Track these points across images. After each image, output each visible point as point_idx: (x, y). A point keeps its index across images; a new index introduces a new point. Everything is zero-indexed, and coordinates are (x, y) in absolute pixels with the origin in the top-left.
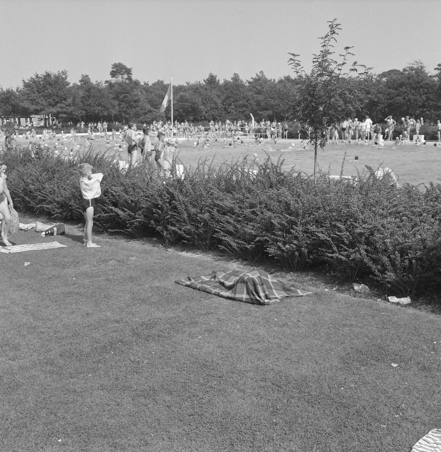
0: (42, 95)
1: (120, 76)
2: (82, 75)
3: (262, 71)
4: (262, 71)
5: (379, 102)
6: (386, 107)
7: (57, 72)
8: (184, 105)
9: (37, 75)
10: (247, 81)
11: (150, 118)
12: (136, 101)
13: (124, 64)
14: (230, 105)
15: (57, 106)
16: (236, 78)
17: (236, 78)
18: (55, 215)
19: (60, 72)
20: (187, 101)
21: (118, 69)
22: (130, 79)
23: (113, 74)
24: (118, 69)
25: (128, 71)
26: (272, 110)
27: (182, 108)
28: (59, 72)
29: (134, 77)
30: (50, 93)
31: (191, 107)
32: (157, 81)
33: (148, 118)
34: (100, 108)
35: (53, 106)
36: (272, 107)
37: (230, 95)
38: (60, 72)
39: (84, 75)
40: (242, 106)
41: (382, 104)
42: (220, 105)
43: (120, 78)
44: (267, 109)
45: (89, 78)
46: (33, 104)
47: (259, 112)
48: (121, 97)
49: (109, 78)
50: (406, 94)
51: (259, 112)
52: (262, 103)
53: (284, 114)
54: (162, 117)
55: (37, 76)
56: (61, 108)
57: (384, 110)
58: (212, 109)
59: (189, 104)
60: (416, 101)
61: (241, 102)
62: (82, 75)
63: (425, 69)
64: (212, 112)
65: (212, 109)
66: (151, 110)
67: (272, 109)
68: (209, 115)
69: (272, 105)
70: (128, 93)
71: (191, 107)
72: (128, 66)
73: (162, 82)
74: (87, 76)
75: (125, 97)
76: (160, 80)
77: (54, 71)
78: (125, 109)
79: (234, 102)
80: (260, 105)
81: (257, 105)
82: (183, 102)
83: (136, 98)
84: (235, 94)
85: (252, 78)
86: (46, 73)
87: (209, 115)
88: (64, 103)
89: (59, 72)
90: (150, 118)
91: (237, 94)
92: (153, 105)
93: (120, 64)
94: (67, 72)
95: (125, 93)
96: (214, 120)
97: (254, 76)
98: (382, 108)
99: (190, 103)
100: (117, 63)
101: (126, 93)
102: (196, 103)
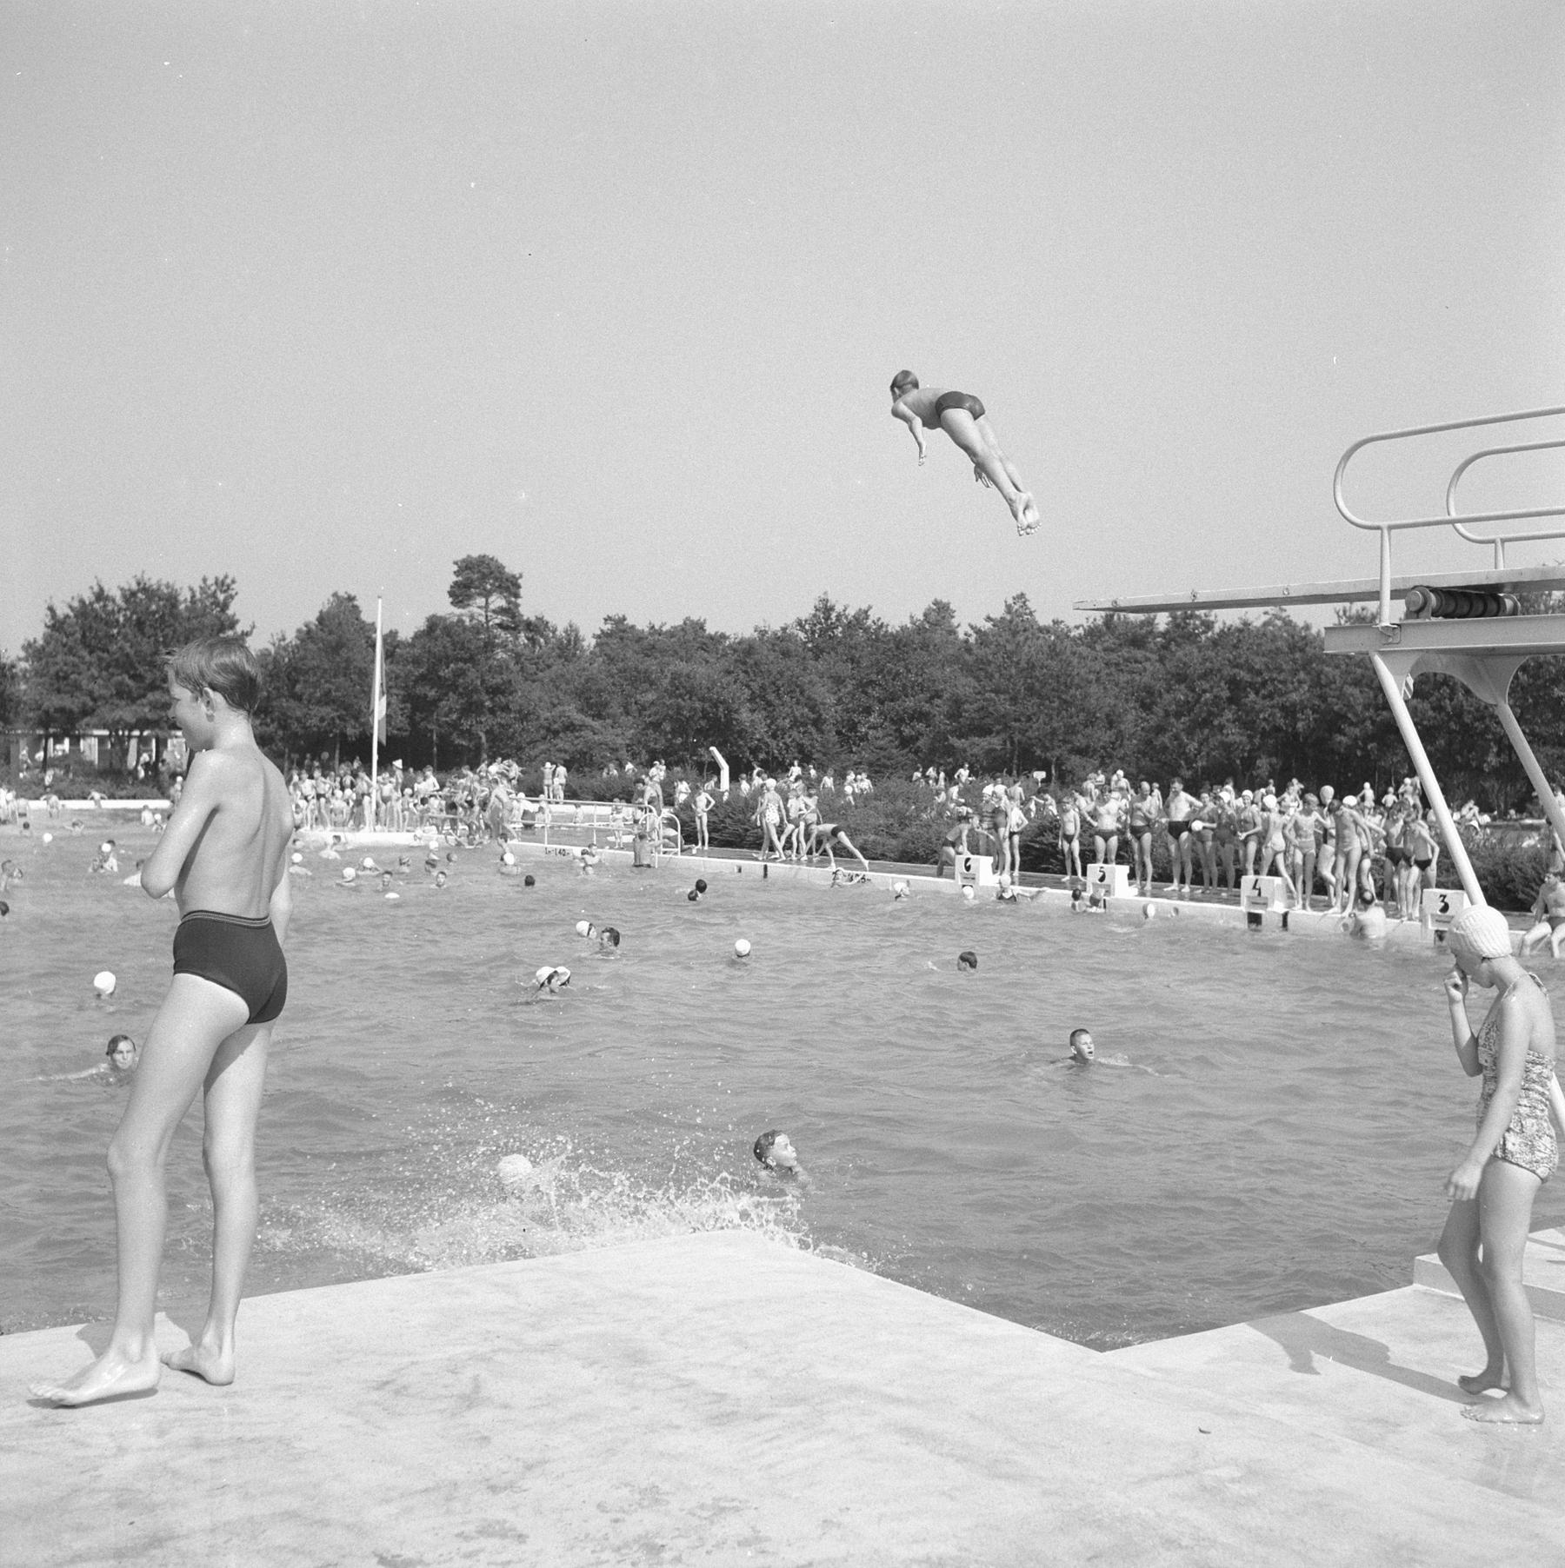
0: (100, 659)
2: (335, 595)
3: (1022, 595)
4: (1022, 595)
5: (1344, 717)
6: (1368, 738)
8: (679, 708)
9: (101, 590)
12: (495, 691)
13: (503, 560)
14: (868, 711)
15: (144, 701)
19: (211, 581)
20: (691, 693)
21: (478, 576)
22: (510, 611)
23: (460, 594)
24: (478, 576)
25: (510, 586)
26: (1003, 736)
28: (205, 580)
29: (528, 608)
30: (127, 655)
33: (560, 751)
34: (328, 711)
36: (1004, 722)
37: (874, 677)
38: (211, 581)
39: (341, 593)
40: (912, 718)
42: (831, 713)
43: (476, 610)
44: (984, 731)
45: (355, 607)
46: (59, 691)
47: (953, 740)
50: (1445, 690)
51: (953, 740)
52: (966, 706)
54: (614, 750)
55: (100, 596)
57: (1364, 749)
58: (795, 724)
59: (698, 705)
61: (910, 703)
62: (335, 595)
63: (873, 615)
65: (795, 724)
68: (787, 747)
70: (471, 659)
72: (511, 568)
73: (699, 626)
74: (351, 599)
75: (461, 673)
76: (695, 618)
78: (454, 716)
79: (882, 702)
82: (681, 696)
83: (498, 680)
84: (889, 672)
85: (989, 619)
87: (787, 747)
89: (205, 580)
91: (898, 674)
93: (482, 560)
95: (457, 660)
96: (805, 760)
98: (1356, 739)
99: (703, 700)
100: (475, 555)
101: (465, 661)
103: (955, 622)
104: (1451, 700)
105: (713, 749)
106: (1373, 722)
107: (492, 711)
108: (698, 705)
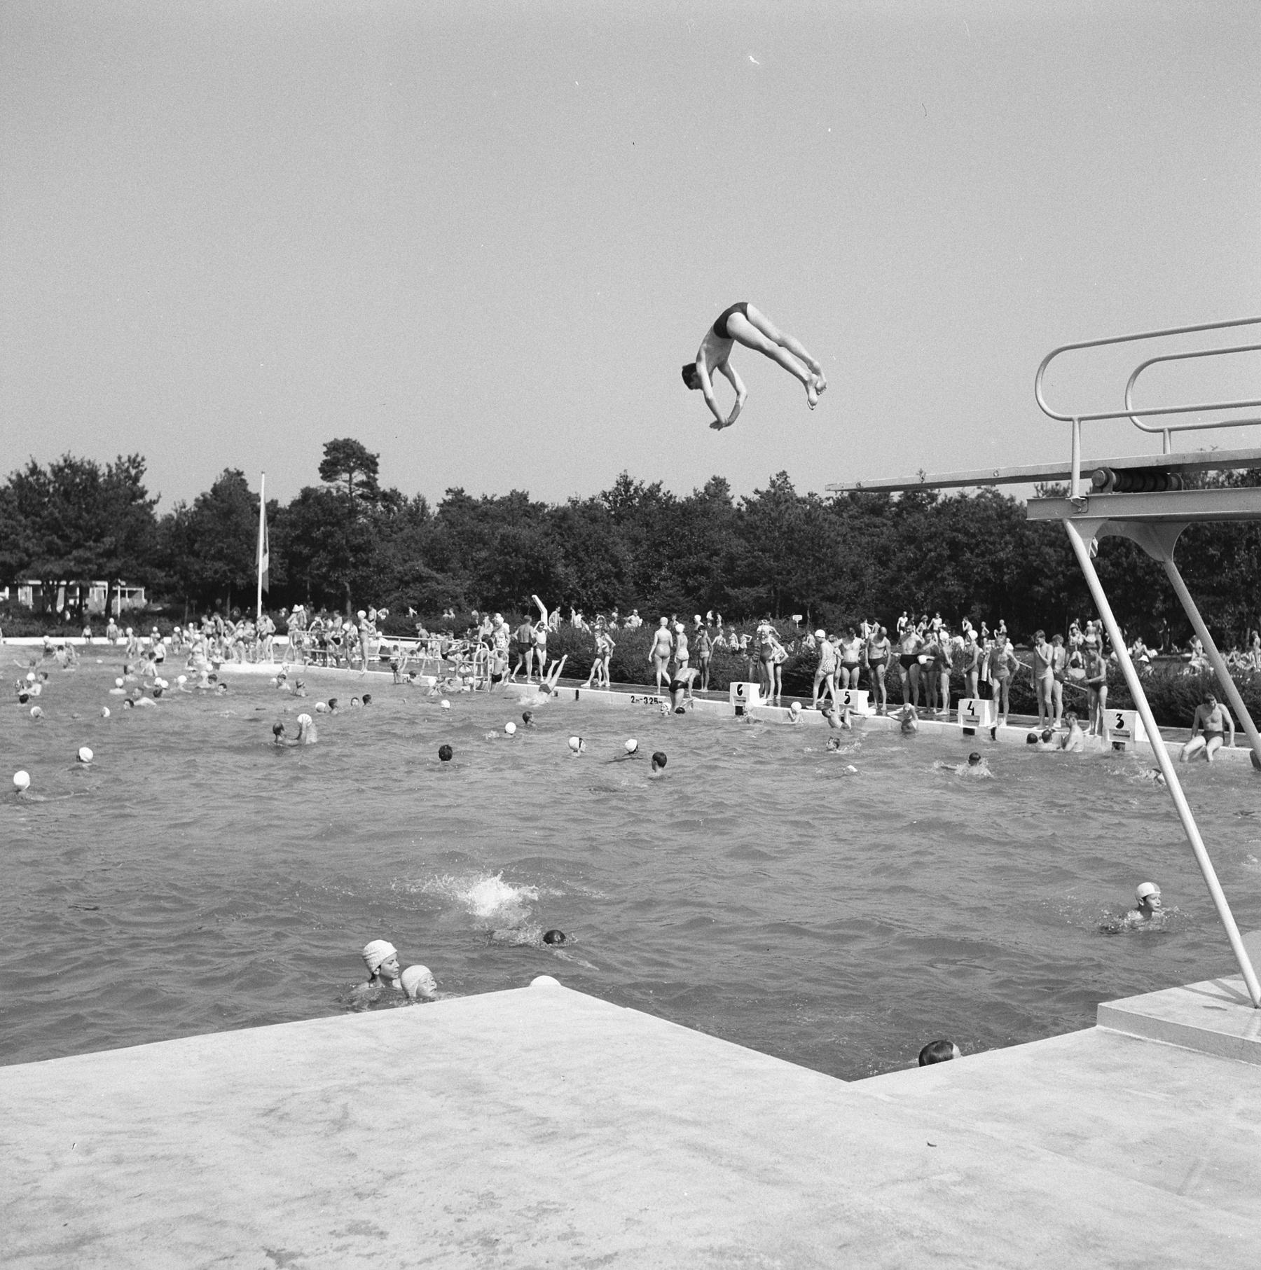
1: (346, 476)
2: (226, 470)
3: (784, 473)
4: (784, 473)
6: (1060, 589)
7: (116, 460)
8: (507, 564)
9: (35, 466)
10: (743, 499)
11: (415, 598)
12: (357, 549)
14: (660, 566)
15: (70, 557)
16: (718, 486)
17: (718, 486)
18: (23, 944)
20: (517, 550)
21: (343, 456)
22: (370, 484)
23: (328, 470)
24: (343, 456)
25: (369, 464)
27: (501, 573)
28: (119, 458)
31: (528, 569)
32: (508, 494)
34: (219, 565)
35: (61, 555)
37: (664, 539)
38: (125, 459)
39: (232, 469)
41: (1047, 577)
42: (630, 568)
44: (753, 583)
47: (728, 590)
48: (317, 534)
49: (316, 481)
51: (728, 590)
52: (739, 562)
53: (802, 597)
54: (455, 597)
55: (34, 470)
56: (78, 561)
57: (1057, 598)
58: (601, 576)
60: (1151, 573)
61: (693, 560)
62: (226, 470)
64: (601, 585)
65: (601, 576)
66: (421, 576)
67: (768, 582)
68: (595, 595)
69: (769, 571)
70: (338, 524)
71: (528, 569)
72: (370, 449)
73: (523, 497)
74: (239, 474)
77: (102, 455)
79: (670, 559)
80: (733, 569)
81: (725, 570)
84: (677, 535)
85: (757, 492)
86: (65, 461)
87: (595, 595)
88: (90, 549)
89: (119, 458)
90: (415, 598)
92: (435, 562)
94: (143, 459)
97: (765, 487)
98: (1050, 589)
99: (526, 556)
100: (341, 439)
101: (333, 525)
102: (543, 559)
103: (730, 494)
104: (1127, 557)
105: (535, 596)
106: (1064, 575)
107: (355, 566)
108: (522, 561)
